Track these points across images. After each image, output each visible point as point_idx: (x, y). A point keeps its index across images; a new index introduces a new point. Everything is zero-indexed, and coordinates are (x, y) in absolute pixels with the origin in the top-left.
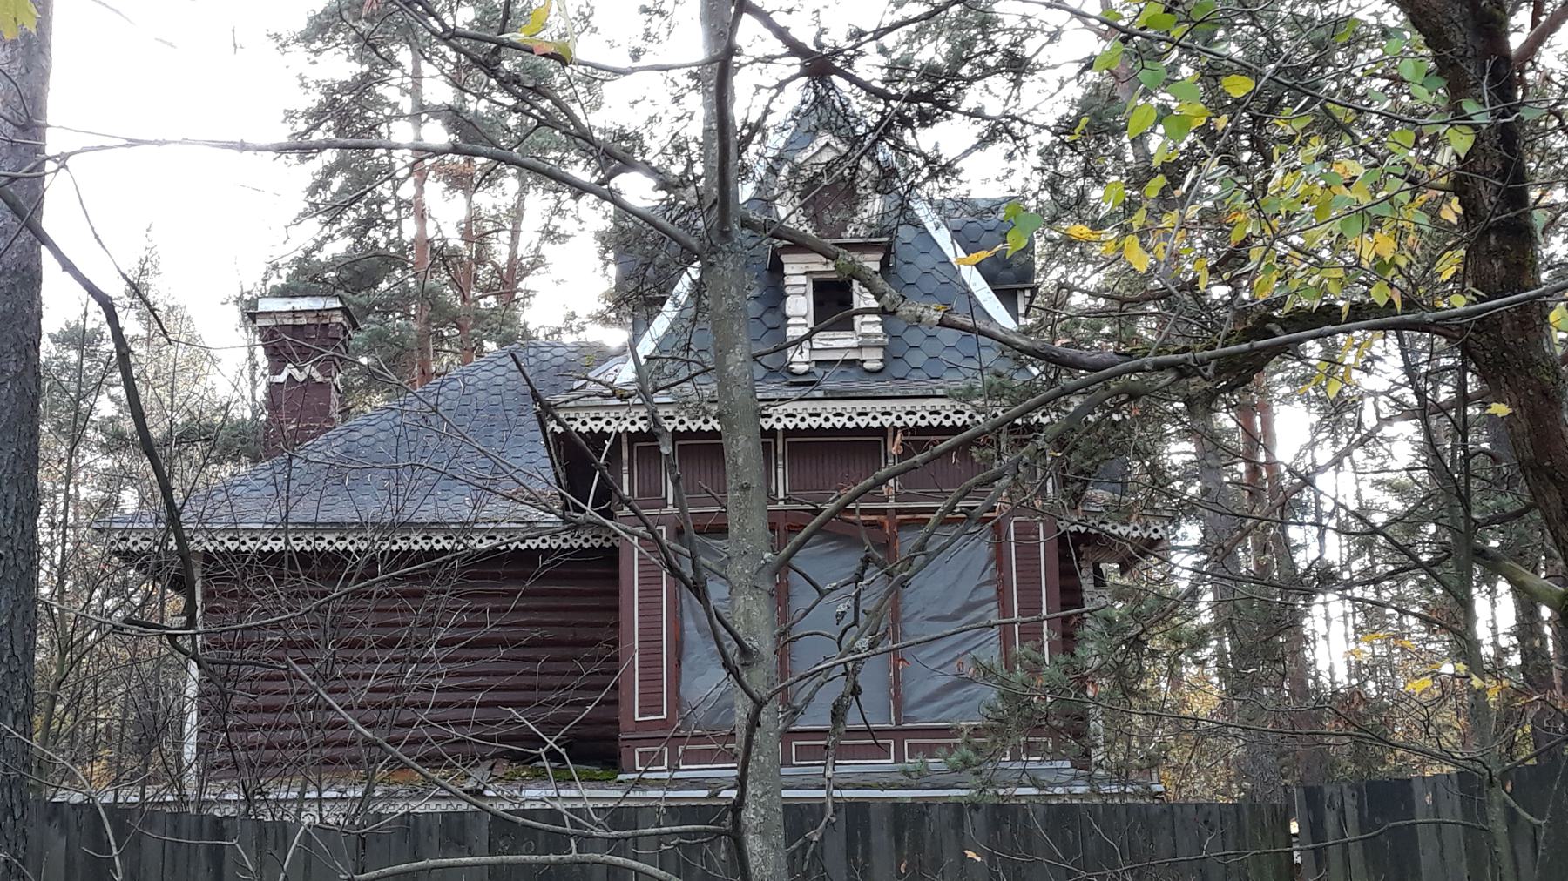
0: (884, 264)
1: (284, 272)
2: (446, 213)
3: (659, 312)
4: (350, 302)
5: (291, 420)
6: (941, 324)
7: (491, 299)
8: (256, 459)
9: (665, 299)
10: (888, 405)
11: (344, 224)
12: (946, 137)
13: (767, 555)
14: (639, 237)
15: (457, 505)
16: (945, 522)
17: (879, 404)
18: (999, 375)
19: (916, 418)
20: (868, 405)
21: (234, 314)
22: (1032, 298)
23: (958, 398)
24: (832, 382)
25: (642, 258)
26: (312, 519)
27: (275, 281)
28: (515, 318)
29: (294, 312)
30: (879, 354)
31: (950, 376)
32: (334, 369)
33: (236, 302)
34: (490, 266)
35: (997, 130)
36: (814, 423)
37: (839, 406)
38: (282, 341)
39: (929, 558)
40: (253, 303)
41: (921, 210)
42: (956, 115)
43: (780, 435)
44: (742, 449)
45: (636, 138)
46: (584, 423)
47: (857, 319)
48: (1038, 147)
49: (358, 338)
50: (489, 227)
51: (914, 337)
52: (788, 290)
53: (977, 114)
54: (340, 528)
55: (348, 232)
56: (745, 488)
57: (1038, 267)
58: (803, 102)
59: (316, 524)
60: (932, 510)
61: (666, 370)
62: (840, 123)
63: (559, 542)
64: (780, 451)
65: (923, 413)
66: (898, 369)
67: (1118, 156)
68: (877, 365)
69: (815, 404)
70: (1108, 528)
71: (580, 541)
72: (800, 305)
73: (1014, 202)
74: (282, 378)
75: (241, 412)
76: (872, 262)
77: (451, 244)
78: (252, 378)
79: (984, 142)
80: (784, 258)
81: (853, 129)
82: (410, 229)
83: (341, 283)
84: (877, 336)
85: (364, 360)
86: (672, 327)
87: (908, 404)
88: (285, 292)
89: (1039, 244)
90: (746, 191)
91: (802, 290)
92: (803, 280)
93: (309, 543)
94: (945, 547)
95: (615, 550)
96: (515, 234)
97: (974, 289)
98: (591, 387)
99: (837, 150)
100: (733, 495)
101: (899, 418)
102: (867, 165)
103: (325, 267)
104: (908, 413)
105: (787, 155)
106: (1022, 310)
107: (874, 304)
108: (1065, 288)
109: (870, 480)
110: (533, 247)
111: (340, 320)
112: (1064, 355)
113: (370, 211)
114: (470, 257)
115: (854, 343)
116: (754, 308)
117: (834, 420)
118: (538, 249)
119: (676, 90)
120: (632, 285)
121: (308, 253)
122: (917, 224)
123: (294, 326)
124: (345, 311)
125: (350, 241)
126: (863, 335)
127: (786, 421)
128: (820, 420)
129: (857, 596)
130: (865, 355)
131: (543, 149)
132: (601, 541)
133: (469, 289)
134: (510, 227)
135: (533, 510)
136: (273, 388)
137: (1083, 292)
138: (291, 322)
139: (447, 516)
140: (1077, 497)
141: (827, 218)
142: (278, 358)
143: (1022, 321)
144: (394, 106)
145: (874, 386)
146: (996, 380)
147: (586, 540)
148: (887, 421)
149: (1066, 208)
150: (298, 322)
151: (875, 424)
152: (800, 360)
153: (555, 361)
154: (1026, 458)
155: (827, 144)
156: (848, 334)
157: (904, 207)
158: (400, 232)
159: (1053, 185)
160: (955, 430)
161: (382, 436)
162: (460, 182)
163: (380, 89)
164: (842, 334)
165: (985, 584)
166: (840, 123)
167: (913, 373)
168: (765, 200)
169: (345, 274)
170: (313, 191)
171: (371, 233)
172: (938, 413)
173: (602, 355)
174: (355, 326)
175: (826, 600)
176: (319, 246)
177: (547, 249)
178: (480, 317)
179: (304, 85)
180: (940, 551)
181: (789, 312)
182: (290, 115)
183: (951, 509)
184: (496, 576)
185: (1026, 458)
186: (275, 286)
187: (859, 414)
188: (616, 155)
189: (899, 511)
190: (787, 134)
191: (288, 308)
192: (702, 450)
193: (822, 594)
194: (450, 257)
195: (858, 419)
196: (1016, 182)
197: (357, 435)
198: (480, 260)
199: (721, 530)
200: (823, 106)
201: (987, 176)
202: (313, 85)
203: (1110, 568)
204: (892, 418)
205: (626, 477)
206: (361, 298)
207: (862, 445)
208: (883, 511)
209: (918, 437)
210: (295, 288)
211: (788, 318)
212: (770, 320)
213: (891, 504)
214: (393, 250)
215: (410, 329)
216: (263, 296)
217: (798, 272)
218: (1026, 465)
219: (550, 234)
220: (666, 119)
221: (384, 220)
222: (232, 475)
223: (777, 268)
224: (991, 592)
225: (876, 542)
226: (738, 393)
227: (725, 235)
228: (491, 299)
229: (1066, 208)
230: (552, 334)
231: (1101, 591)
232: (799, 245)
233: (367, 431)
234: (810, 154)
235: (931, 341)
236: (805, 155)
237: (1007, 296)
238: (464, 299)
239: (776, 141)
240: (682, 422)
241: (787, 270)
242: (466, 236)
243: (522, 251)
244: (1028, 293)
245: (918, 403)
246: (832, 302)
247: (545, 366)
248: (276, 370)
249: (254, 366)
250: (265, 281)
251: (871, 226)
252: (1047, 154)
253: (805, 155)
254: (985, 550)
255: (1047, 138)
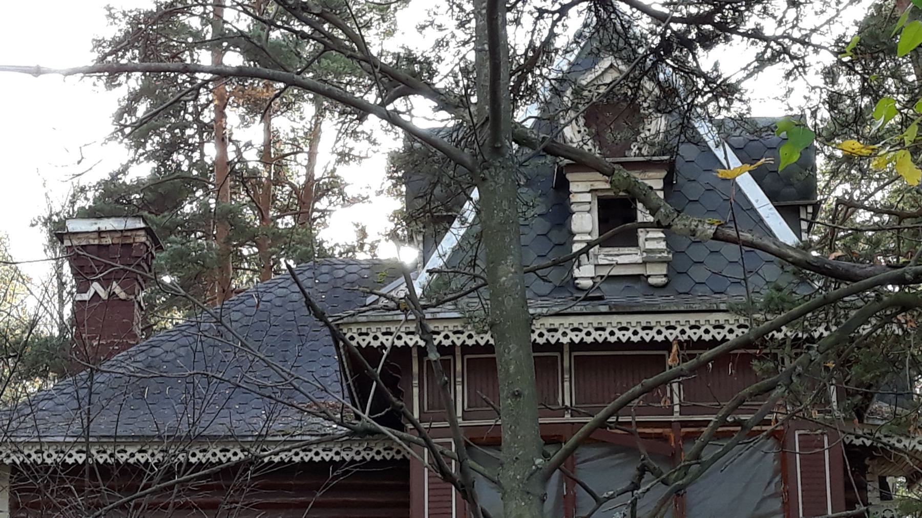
0: (668, 183)
1: (90, 195)
2: (247, 134)
3: (447, 230)
4: (153, 223)
5: (98, 332)
6: (715, 237)
7: (289, 220)
8: (62, 376)
9: (454, 218)
10: (672, 319)
11: (149, 147)
12: (728, 58)
13: (538, 461)
14: (426, 156)
15: (250, 418)
16: (717, 436)
17: (663, 319)
18: (779, 290)
19: (700, 332)
20: (652, 319)
21: (42, 236)
22: (815, 214)
23: (738, 312)
24: (615, 295)
25: (429, 177)
26: (112, 433)
27: (81, 203)
28: (312, 238)
29: (100, 233)
30: (663, 269)
31: (733, 291)
32: (137, 287)
33: (45, 224)
34: (288, 187)
35: (775, 52)
36: (599, 336)
37: (624, 320)
38: (86, 258)
39: (704, 466)
40: (62, 223)
41: (703, 129)
42: (734, 36)
43: (566, 349)
44: (514, 364)
45: (427, 64)
46: (375, 338)
47: (642, 234)
48: (820, 67)
49: (161, 257)
50: (287, 149)
51: (698, 253)
52: (574, 208)
53: (756, 34)
54: (143, 441)
55: (151, 156)
56: (517, 395)
57: (821, 184)
58: (586, 25)
59: (116, 437)
60: (706, 423)
61: (453, 286)
62: (621, 45)
63: (352, 454)
64: (566, 364)
65: (705, 326)
66: (682, 284)
67: (896, 74)
68: (661, 280)
69: (600, 319)
70: (893, 441)
71: (372, 454)
72: (584, 223)
73: (797, 122)
74: (86, 297)
75: (49, 329)
76: (654, 181)
77: (251, 165)
78: (60, 297)
79: (762, 62)
80: (569, 177)
81: (634, 52)
82: (211, 151)
83: (145, 204)
84: (661, 251)
85: (167, 279)
86: (459, 244)
87: (692, 319)
88: (92, 214)
89: (820, 160)
90: (526, 114)
91: (587, 207)
92: (588, 198)
93: (111, 455)
94: (719, 456)
95: (405, 462)
96: (312, 156)
97: (756, 205)
98: (384, 302)
99: (620, 72)
100: (506, 402)
101: (683, 332)
102: (648, 85)
103: (131, 189)
104: (691, 328)
105: (572, 76)
106: (804, 225)
107: (651, 219)
108: (849, 205)
109: (638, 388)
110: (330, 168)
111: (143, 239)
112: (836, 268)
113: (174, 135)
114: (268, 178)
115: (638, 258)
116: (541, 226)
117: (619, 334)
118: (334, 170)
119: (462, 15)
120: (421, 202)
121: (114, 176)
122: (698, 141)
123: (99, 246)
124: (148, 231)
125: (153, 164)
126: (648, 251)
127: (572, 335)
128: (606, 334)
129: (634, 504)
130: (650, 270)
131: (338, 75)
132: (392, 453)
133: (268, 209)
134: (307, 149)
135: (326, 423)
136: (79, 306)
137: (868, 209)
138: (96, 242)
139: (241, 428)
140: (860, 412)
141: (608, 136)
142: (83, 275)
143: (805, 237)
144: (196, 34)
145: (659, 300)
146: (775, 294)
147: (378, 453)
148: (671, 335)
149: (845, 125)
150: (104, 242)
151: (659, 338)
152: (585, 273)
153: (350, 278)
154: (799, 369)
155: (611, 66)
156: (633, 250)
157: (685, 126)
158: (202, 155)
159: (833, 101)
160: (714, 342)
161: (182, 351)
162: (262, 109)
163: (184, 18)
164: (626, 250)
165: (770, 496)
166: (621, 45)
167: (697, 287)
168: (549, 119)
169: (150, 196)
170: (119, 116)
171: (175, 156)
172: (722, 327)
173: (396, 271)
174: (160, 248)
175: (605, 507)
176: (124, 170)
177: (343, 171)
178: (277, 236)
179: (111, 16)
180: (715, 459)
181: (575, 227)
182: (99, 43)
183: (723, 422)
184: (289, 488)
185: (799, 369)
186: (83, 208)
187: (644, 328)
188: (405, 77)
189: (684, 424)
190: (572, 58)
191: (94, 228)
192: (481, 361)
193: (599, 502)
194: (249, 178)
195: (642, 333)
196: (797, 103)
197: (158, 351)
198: (279, 180)
199: (495, 443)
200: (606, 29)
201: (770, 97)
202: (121, 16)
203: (897, 482)
204: (676, 332)
205: (416, 391)
206: (164, 219)
207: (646, 357)
208: (669, 424)
209: (691, 346)
210: (101, 210)
211: (574, 235)
212: (556, 237)
213: (676, 417)
214: (195, 173)
215: (210, 248)
216: (71, 217)
217: (583, 190)
218: (799, 375)
219: (344, 157)
220: (453, 44)
221: (186, 143)
222: (40, 390)
223: (563, 186)
224: (776, 504)
225: (663, 455)
226: (509, 303)
227: (497, 151)
228: (289, 220)
229: (845, 125)
230: (347, 252)
231: (886, 504)
232: (581, 163)
233: (168, 346)
234: (593, 76)
235: (714, 256)
236: (590, 77)
237: (789, 213)
238: (263, 219)
239: (561, 63)
240: (470, 336)
241: (573, 187)
242: (265, 156)
243: (318, 174)
244: (810, 210)
245: (702, 318)
246: (617, 219)
247: (339, 283)
248: (82, 287)
249: (62, 285)
250: (73, 203)
251: (652, 145)
252: (830, 75)
253: (590, 77)
254: (771, 461)
255: (828, 59)
